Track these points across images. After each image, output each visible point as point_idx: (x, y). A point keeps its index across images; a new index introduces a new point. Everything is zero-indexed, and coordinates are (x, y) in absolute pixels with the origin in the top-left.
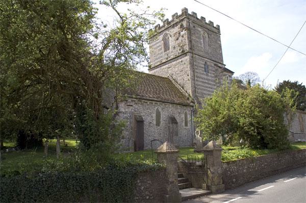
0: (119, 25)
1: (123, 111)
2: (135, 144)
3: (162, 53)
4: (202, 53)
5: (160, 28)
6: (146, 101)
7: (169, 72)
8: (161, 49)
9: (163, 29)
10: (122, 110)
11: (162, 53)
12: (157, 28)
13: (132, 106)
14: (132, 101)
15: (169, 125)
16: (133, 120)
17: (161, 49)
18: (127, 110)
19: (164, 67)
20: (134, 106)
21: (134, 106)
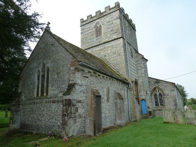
0: (9, 122)
1: (80, 82)
2: (95, 125)
3: (93, 38)
4: (107, 46)
5: (92, 18)
6: (100, 74)
7: (101, 54)
8: (92, 35)
9: (95, 18)
10: (79, 81)
11: (93, 38)
12: (90, 18)
13: (87, 77)
14: (89, 72)
15: (115, 101)
16: (90, 95)
17: (92, 35)
18: (83, 82)
19: (97, 49)
20: (90, 78)
21: (90, 78)
